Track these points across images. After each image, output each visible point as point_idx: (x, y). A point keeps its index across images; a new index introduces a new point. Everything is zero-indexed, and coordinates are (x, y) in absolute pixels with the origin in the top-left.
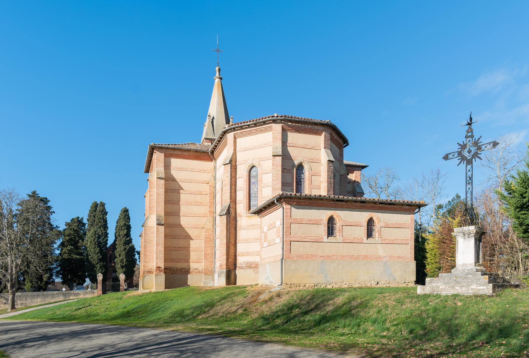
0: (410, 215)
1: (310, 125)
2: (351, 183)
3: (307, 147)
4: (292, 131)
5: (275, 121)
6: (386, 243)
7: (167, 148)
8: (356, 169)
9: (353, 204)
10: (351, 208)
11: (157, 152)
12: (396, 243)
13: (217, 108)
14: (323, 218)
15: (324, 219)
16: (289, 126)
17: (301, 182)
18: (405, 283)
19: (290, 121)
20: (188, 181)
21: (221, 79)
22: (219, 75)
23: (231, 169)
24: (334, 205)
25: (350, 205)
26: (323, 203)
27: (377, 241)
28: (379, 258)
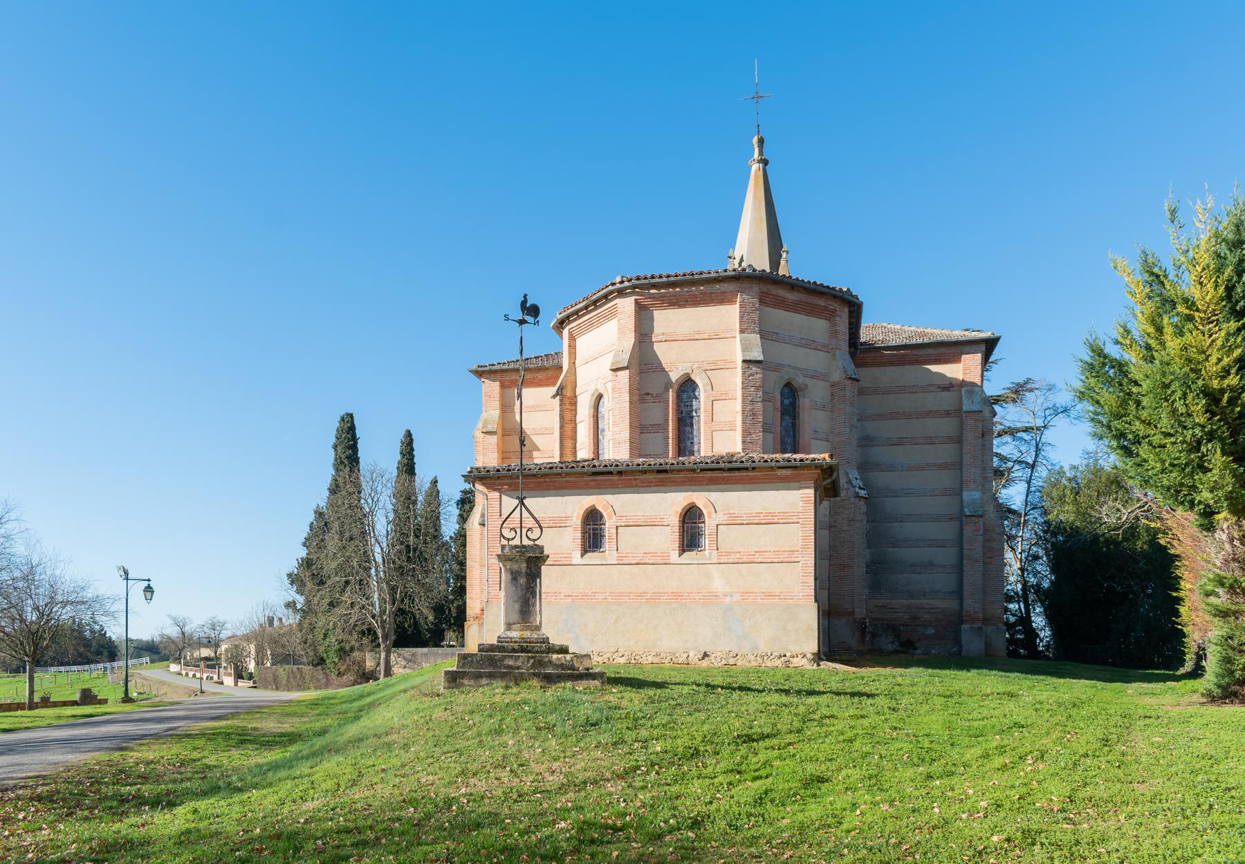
0: (800, 492)
1: (702, 286)
2: (955, 389)
3: (699, 338)
4: (661, 307)
5: (621, 293)
6: (732, 561)
7: (503, 371)
8: (967, 349)
9: (637, 477)
10: (637, 486)
11: (486, 380)
12: (759, 560)
13: (750, 233)
14: (573, 513)
15: (575, 514)
16: (653, 297)
17: (692, 417)
18: (783, 658)
19: (654, 286)
20: (547, 432)
21: (765, 162)
22: (761, 153)
23: (560, 405)
24: (593, 483)
25: (631, 479)
26: (567, 482)
27: (707, 559)
28: (710, 598)
